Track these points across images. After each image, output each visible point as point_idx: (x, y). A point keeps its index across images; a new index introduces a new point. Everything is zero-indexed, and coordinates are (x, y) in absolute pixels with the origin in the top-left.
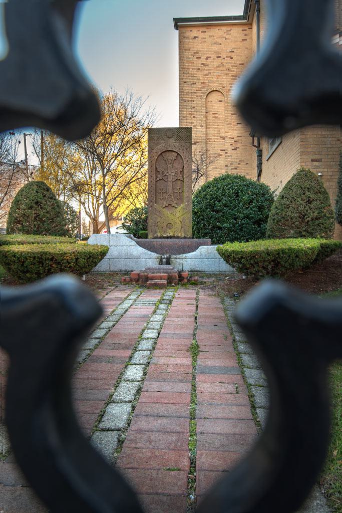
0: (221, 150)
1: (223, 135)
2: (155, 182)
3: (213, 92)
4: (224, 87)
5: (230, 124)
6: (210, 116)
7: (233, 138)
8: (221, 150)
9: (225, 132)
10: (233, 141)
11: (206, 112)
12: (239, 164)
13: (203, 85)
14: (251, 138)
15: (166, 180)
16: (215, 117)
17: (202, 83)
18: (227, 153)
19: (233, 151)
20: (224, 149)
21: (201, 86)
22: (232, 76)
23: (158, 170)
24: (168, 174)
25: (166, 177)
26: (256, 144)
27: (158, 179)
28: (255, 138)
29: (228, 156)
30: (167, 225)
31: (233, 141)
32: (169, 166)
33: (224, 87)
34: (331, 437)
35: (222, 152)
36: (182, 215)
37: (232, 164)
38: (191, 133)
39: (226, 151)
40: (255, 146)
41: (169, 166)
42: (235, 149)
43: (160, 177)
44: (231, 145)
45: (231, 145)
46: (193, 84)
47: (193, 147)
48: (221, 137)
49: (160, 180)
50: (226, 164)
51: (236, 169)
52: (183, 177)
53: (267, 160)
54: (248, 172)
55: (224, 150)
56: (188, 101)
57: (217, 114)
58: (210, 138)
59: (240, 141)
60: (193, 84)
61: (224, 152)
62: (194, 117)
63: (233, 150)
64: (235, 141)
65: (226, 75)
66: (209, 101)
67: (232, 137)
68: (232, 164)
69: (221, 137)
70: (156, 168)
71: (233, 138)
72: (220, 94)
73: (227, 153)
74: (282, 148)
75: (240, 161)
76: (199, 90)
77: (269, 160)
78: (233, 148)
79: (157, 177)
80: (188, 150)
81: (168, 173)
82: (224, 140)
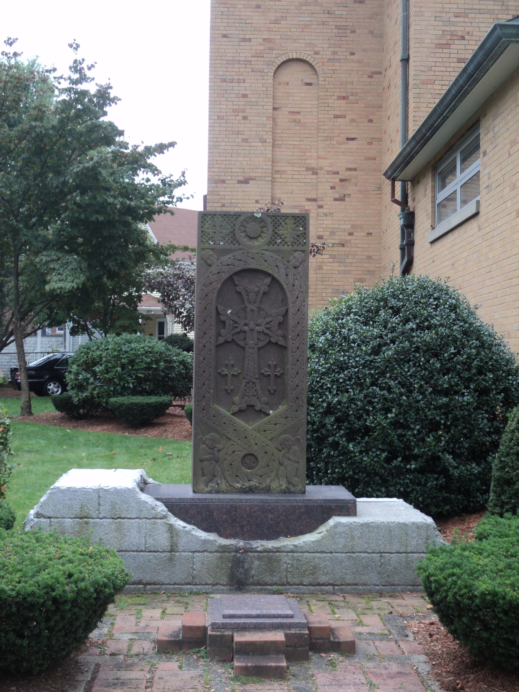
0: (309, 200)
1: (313, 163)
2: (213, 348)
3: (290, 63)
4: (316, 53)
5: (331, 138)
6: (283, 118)
7: (338, 173)
8: (309, 200)
9: (319, 158)
10: (336, 179)
11: (274, 109)
12: (351, 234)
13: (270, 45)
14: (389, 182)
15: (242, 343)
16: (295, 121)
17: (264, 40)
18: (321, 207)
19: (337, 203)
20: (314, 197)
21: (262, 48)
22: (338, 27)
23: (222, 318)
24: (246, 328)
25: (242, 335)
26: (398, 196)
27: (221, 340)
28: (396, 183)
29: (326, 215)
30: (244, 457)
31: (336, 179)
32: (250, 307)
33: (316, 53)
34: (145, 234)
35: (310, 203)
36: (281, 434)
37: (332, 233)
38: (306, 226)
39: (320, 203)
40: (396, 201)
41: (250, 307)
42: (342, 199)
43: (226, 334)
44: (332, 188)
45: (332, 188)
46: (245, 40)
47: (313, 261)
48: (308, 169)
49: (226, 342)
50: (320, 234)
51: (343, 245)
52: (284, 337)
53: (432, 242)
54: (371, 254)
55: (315, 200)
56: (232, 81)
57: (299, 113)
58: (283, 169)
59: (353, 180)
60: (245, 40)
61: (314, 203)
62: (245, 118)
63: (336, 200)
64: (342, 180)
65: (323, 23)
66: (280, 84)
67: (335, 169)
68: (332, 233)
69: (308, 169)
70: (218, 313)
71: (338, 173)
72: (306, 67)
73: (321, 207)
74: (480, 229)
75: (353, 227)
76: (258, 55)
77: (439, 244)
78: (337, 196)
79: (219, 335)
80: (300, 269)
81: (246, 325)
82: (315, 177)
